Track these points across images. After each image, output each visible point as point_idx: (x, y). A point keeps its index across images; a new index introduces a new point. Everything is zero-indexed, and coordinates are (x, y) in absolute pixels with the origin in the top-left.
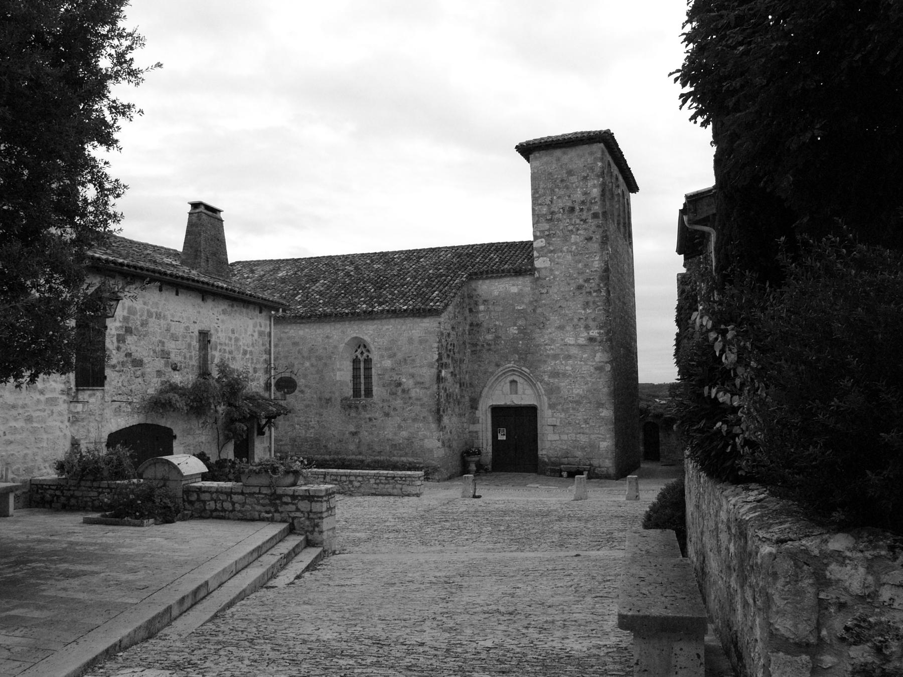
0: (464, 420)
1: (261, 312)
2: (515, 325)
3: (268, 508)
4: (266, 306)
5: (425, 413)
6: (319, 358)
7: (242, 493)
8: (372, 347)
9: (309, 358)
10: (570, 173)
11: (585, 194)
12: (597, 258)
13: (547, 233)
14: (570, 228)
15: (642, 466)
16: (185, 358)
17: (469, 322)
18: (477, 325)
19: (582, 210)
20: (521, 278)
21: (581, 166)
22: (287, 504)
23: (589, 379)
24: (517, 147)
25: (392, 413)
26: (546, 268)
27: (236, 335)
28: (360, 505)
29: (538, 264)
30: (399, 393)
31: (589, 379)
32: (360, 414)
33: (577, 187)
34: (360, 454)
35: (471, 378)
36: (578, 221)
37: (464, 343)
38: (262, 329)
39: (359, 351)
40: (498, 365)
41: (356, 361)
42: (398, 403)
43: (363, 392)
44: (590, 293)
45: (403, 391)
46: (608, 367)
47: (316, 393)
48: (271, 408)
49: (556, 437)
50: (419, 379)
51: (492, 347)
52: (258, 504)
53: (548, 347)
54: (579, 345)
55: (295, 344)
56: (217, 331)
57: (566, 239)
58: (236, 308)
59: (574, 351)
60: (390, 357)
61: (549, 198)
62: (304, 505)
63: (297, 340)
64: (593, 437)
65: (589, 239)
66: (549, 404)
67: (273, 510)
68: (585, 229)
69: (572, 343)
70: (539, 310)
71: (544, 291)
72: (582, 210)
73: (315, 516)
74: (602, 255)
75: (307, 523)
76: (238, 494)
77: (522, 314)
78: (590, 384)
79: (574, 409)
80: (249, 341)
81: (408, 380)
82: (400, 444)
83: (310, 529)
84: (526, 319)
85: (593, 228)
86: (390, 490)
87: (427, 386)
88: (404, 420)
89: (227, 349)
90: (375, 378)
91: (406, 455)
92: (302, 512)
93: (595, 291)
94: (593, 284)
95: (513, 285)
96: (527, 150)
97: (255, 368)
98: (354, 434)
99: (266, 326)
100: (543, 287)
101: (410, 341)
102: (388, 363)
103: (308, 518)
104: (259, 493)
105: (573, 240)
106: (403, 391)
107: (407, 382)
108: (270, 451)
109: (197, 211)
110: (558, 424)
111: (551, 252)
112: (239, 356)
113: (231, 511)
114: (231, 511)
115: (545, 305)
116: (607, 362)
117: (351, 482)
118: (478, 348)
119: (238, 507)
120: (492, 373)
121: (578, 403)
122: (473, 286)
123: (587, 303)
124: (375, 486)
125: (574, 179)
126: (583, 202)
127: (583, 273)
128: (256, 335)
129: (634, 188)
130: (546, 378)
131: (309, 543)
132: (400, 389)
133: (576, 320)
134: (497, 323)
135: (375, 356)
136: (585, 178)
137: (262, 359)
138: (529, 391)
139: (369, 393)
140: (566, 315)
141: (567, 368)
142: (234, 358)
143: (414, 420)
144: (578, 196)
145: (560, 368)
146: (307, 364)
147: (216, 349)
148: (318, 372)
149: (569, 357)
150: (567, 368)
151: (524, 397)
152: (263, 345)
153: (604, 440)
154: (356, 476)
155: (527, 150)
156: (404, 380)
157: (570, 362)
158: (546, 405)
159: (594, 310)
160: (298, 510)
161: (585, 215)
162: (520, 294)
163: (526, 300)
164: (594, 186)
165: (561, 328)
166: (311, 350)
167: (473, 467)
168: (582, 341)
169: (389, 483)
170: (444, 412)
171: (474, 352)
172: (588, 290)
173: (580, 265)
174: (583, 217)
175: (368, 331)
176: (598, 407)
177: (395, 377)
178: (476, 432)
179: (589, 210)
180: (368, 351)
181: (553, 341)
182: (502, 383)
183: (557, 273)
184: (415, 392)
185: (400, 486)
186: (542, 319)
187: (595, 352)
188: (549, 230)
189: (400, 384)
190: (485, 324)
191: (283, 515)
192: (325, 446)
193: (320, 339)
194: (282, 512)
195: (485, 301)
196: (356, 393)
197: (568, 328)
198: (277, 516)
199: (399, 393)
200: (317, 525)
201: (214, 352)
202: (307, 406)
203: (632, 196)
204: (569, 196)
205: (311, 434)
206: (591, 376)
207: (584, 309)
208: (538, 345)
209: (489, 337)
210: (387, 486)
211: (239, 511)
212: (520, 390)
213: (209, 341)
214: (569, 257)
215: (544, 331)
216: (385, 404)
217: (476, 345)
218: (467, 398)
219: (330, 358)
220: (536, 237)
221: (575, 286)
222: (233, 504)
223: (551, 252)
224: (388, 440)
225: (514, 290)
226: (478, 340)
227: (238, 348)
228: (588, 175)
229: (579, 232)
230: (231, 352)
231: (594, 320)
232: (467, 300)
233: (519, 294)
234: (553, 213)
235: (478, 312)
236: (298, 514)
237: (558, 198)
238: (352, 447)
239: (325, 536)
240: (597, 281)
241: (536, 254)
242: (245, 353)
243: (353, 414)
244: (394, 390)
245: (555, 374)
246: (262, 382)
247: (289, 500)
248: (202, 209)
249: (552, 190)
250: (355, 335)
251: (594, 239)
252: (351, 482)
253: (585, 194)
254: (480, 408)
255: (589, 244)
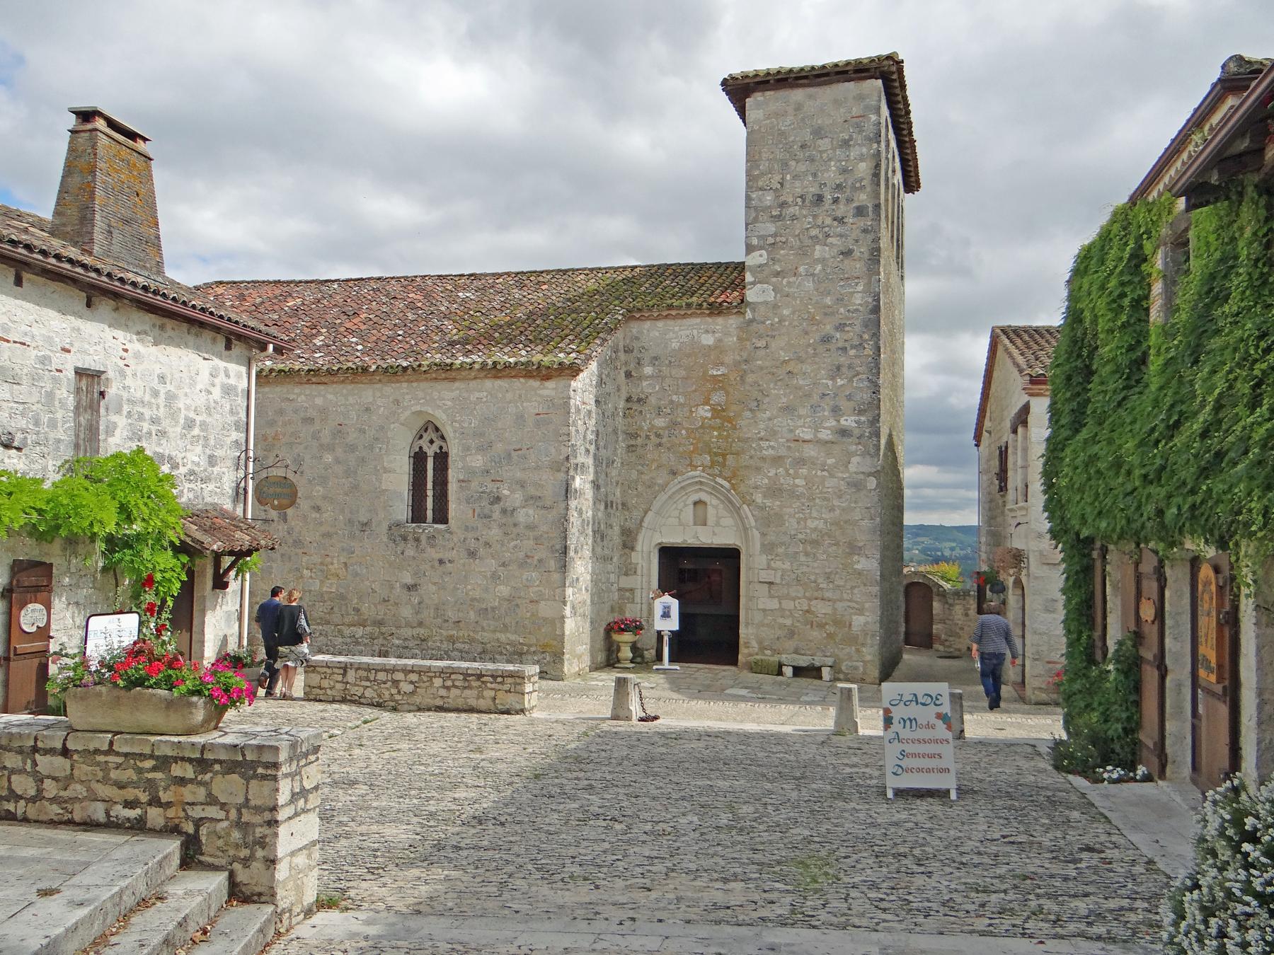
0: (610, 567)
1: (228, 347)
2: (706, 403)
3: (130, 793)
4: (240, 337)
5: (542, 553)
6: (352, 448)
7: (65, 752)
8: (448, 431)
9: (330, 448)
10: (818, 133)
11: (844, 171)
12: (860, 288)
13: (771, 240)
14: (814, 232)
15: (905, 656)
16: (37, 424)
17: (624, 395)
18: (639, 400)
19: (836, 201)
20: (720, 320)
21: (840, 120)
22: (182, 781)
23: (836, 503)
24: (725, 83)
25: (482, 551)
26: (766, 303)
27: (169, 387)
28: (408, 733)
29: (751, 295)
30: (496, 515)
31: (836, 503)
32: (423, 551)
33: (830, 160)
34: (420, 624)
35: (624, 492)
36: (828, 221)
37: (615, 432)
38: (232, 381)
39: (426, 437)
40: (674, 473)
41: (419, 459)
42: (495, 533)
43: (430, 513)
44: (844, 349)
45: (504, 511)
46: (872, 483)
47: (342, 511)
48: (238, 535)
49: (774, 604)
50: (532, 491)
51: (664, 440)
52: (105, 780)
53: (764, 444)
54: (819, 442)
55: (309, 421)
56: (123, 374)
57: (803, 252)
58: (170, 333)
59: (810, 451)
60: (480, 449)
61: (778, 178)
62: (228, 787)
63: (312, 413)
64: (839, 605)
65: (847, 253)
66: (763, 545)
67: (144, 798)
68: (841, 236)
69: (807, 437)
70: (750, 378)
71: (761, 343)
72: (836, 201)
73: (257, 819)
74: (870, 282)
75: (236, 835)
76: (50, 751)
77: (719, 383)
78: (837, 512)
79: (807, 554)
80: (201, 400)
81: (512, 492)
82: (493, 609)
83: (245, 853)
84: (727, 393)
85: (856, 233)
86: (473, 702)
87: (548, 503)
88: (503, 565)
89: (147, 413)
90: (452, 487)
91: (505, 628)
92: (223, 806)
93: (853, 347)
94: (852, 334)
95: (707, 332)
96: (740, 90)
97: (210, 457)
98: (411, 588)
99: (239, 376)
100: (760, 337)
101: (520, 418)
102: (477, 461)
103: (238, 824)
104: (110, 751)
105: (817, 254)
106: (504, 511)
107: (515, 498)
108: (240, 619)
109: (89, 126)
110: (778, 581)
111: (777, 274)
112: (175, 431)
113: (33, 800)
114: (33, 800)
115: (761, 368)
116: (870, 474)
117: (396, 683)
118: (639, 441)
119: (50, 788)
120: (663, 488)
121: (815, 543)
122: (634, 331)
123: (838, 368)
124: (443, 692)
125: (824, 144)
126: (839, 187)
127: (832, 314)
128: (217, 393)
129: (911, 183)
130: (759, 498)
131: (238, 894)
132: (497, 507)
133: (816, 397)
134: (675, 398)
135: (454, 451)
136: (846, 144)
137: (229, 440)
138: (728, 521)
139: (441, 516)
140: (799, 388)
141: (797, 481)
142: (162, 433)
143: (523, 565)
144: (831, 175)
145: (786, 482)
146: (329, 458)
147: (119, 412)
148: (348, 473)
149: (801, 462)
150: (797, 481)
151: (716, 533)
152: (232, 412)
153: (861, 611)
154: (407, 671)
155: (740, 90)
156: (506, 492)
157: (804, 471)
158: (758, 546)
159: (851, 380)
160: (212, 800)
161: (841, 210)
162: (718, 347)
163: (728, 359)
164: (862, 158)
165: (788, 409)
166: (339, 431)
167: (626, 653)
168: (825, 435)
169: (470, 687)
170: (576, 552)
171: (631, 449)
172: (840, 344)
173: (828, 301)
174: (839, 214)
175: (441, 402)
176: (851, 554)
177: (491, 486)
178: (632, 590)
179: (849, 201)
180: (443, 437)
181: (773, 433)
182: (681, 505)
183: (786, 312)
184: (525, 515)
185: (492, 693)
186: (755, 394)
187: (850, 455)
188: (775, 235)
189: (498, 499)
190: (653, 400)
191: (171, 813)
192: (357, 610)
193: (353, 414)
194: (169, 805)
195: (656, 358)
196: (418, 515)
197: (802, 411)
198: (155, 816)
199: (496, 515)
200: (262, 842)
201: (114, 418)
202: (327, 535)
203: (908, 199)
204: (815, 175)
205: (331, 586)
206: (840, 497)
207: (833, 378)
208: (746, 440)
209: (660, 422)
210: (467, 692)
211: (53, 800)
212: (711, 519)
213: (102, 394)
214: (809, 285)
215: (760, 415)
216: (470, 535)
217: (634, 436)
218: (617, 529)
219: (371, 448)
220: (750, 249)
221: (817, 337)
222: (40, 780)
223: (777, 274)
224: (473, 600)
225: (708, 340)
226: (641, 428)
227: (173, 415)
228: (851, 139)
229: (830, 240)
230: (154, 421)
231: (849, 398)
232: (622, 355)
233: (716, 347)
234: (783, 205)
235: (640, 378)
236: (213, 812)
237: (795, 177)
238: (406, 612)
239: (282, 872)
240: (858, 328)
241: (749, 277)
242: (190, 424)
243: (410, 552)
244: (486, 511)
245: (774, 491)
246: (228, 488)
247: (189, 771)
248: (100, 124)
249: (785, 164)
250: (418, 408)
251: (857, 254)
252: (396, 683)
253: (844, 171)
254: (639, 548)
255: (846, 262)
